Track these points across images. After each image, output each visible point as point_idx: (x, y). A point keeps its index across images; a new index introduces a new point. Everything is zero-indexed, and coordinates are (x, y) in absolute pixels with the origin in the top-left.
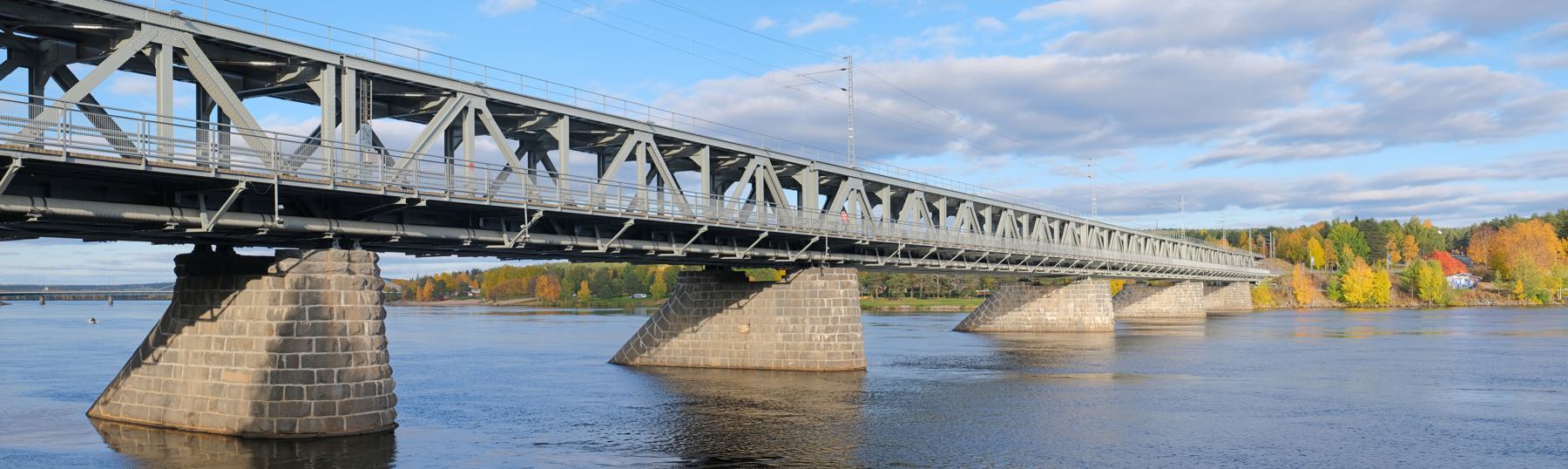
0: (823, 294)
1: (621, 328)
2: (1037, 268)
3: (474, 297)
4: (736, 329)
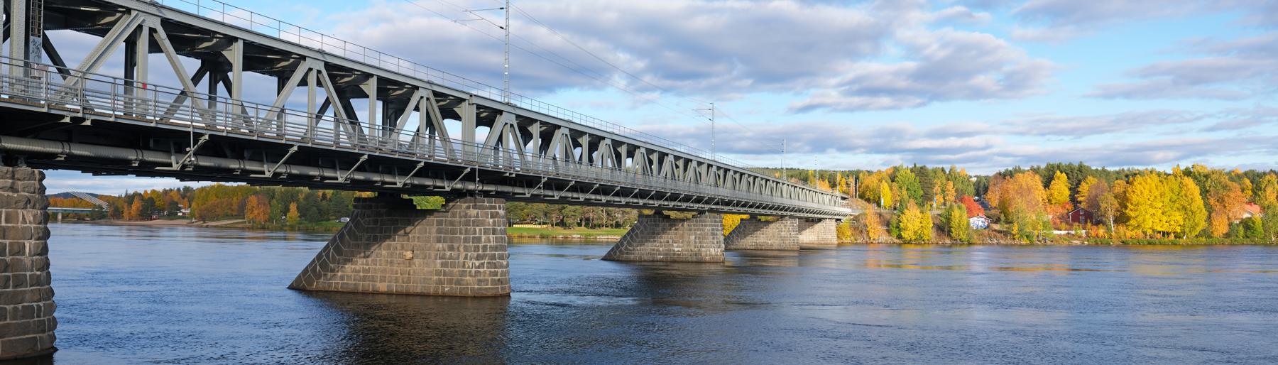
0: (476, 223)
1: (296, 254)
2: (661, 202)
3: (184, 217)
4: (401, 256)
